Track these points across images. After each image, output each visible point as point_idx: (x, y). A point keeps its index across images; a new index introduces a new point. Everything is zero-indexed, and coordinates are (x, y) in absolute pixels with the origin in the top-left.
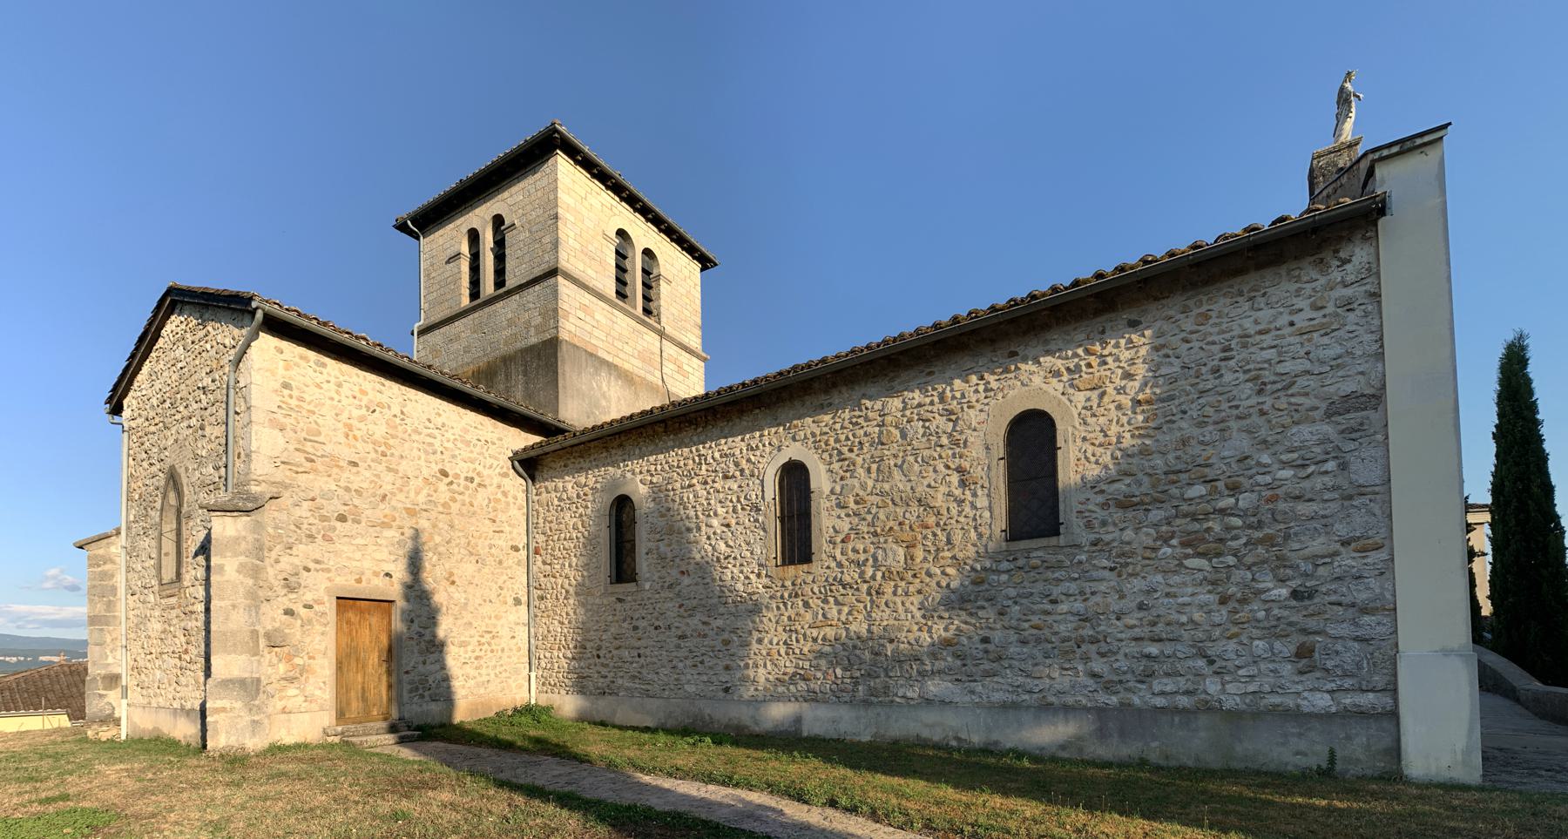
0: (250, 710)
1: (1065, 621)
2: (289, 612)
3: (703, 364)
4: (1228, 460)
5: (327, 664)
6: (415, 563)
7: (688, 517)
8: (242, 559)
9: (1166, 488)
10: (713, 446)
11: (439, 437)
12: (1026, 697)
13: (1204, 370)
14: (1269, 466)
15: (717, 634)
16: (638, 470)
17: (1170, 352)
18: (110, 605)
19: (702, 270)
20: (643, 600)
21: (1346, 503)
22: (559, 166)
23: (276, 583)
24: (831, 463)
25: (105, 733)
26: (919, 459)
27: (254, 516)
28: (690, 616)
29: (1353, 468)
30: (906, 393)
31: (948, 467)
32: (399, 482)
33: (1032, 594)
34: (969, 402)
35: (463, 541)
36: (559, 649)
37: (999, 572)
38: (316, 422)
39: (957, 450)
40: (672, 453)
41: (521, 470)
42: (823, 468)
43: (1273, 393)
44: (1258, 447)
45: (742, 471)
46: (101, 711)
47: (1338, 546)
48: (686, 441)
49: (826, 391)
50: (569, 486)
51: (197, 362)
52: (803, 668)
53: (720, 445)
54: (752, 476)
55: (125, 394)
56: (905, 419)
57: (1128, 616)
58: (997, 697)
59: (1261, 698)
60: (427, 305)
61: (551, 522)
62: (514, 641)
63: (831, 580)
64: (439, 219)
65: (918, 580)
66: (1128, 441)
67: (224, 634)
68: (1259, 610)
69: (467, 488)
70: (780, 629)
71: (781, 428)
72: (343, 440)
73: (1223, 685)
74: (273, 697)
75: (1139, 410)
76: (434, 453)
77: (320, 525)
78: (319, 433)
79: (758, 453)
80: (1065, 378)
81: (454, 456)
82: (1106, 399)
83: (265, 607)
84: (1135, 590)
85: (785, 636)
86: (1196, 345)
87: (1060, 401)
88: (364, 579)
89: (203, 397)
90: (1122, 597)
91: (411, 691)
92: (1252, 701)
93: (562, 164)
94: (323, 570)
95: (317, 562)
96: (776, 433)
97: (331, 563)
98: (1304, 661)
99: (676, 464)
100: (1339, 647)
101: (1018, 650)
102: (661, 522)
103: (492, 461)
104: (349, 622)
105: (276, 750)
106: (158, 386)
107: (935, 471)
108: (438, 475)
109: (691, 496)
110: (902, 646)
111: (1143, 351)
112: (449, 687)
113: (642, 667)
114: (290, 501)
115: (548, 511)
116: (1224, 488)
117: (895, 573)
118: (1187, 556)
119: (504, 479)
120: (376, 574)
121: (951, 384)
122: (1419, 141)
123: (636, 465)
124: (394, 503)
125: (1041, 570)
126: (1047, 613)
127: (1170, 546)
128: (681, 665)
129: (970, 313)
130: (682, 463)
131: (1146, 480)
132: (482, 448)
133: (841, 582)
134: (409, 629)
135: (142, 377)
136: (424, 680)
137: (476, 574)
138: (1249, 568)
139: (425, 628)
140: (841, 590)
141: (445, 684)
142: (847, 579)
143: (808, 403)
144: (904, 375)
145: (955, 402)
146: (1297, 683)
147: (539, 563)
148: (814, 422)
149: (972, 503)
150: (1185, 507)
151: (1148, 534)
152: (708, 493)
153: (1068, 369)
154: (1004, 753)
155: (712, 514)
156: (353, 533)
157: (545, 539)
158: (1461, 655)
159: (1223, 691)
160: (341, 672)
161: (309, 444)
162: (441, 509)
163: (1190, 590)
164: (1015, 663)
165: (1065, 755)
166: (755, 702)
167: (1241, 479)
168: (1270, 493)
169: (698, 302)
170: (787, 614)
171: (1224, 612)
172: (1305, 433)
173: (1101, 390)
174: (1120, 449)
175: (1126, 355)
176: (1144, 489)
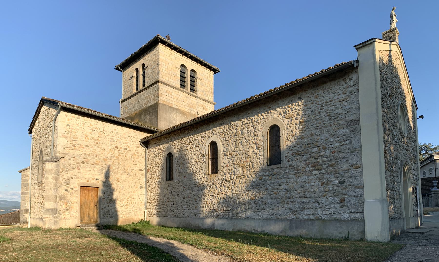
0: (54, 218)
1: (282, 191)
2: (66, 190)
3: (214, 106)
4: (323, 140)
5: (77, 206)
6: (107, 175)
7: (186, 159)
8: (53, 175)
9: (308, 149)
11: (115, 137)
12: (272, 216)
13: (317, 112)
14: (333, 142)
15: (193, 197)
16: (174, 145)
17: (308, 107)
18: (27, 189)
19: (214, 74)
21: (352, 153)
22: (160, 48)
23: (62, 182)
24: (223, 142)
25: (24, 226)
26: (246, 140)
27: (57, 163)
28: (187, 191)
29: (353, 142)
30: (243, 120)
31: (253, 143)
32: (102, 151)
33: (274, 183)
34: (259, 122)
35: (123, 168)
36: (153, 203)
37: (266, 176)
38: (76, 135)
39: (256, 137)
42: (221, 143)
43: (334, 119)
44: (330, 136)
45: (200, 144)
46: (24, 219)
47: (350, 167)
48: (186, 135)
49: (222, 119)
50: (157, 150)
51: (48, 119)
52: (215, 208)
54: (203, 146)
55: (33, 128)
56: (242, 128)
57: (298, 190)
58: (265, 216)
59: (332, 215)
61: (152, 161)
62: (140, 200)
63: (223, 179)
64: (128, 65)
65: (245, 179)
66: (298, 134)
67: (48, 196)
68: (331, 187)
70: (210, 195)
71: (210, 131)
72: (84, 140)
73: (322, 211)
74: (61, 214)
75: (301, 124)
76: (114, 141)
77: (76, 165)
78: (77, 138)
79: (204, 139)
80: (283, 115)
81: (120, 142)
82: (293, 121)
83: (59, 189)
84: (300, 181)
85: (211, 197)
86: (315, 105)
87: (281, 122)
88: (89, 180)
89: (48, 129)
90: (297, 183)
91: (103, 215)
92: (329, 216)
93: (161, 47)
94: (77, 178)
95: (75, 176)
96: (209, 132)
97: (79, 176)
98: (342, 203)
99: (183, 143)
100: (350, 199)
101: (270, 201)
102: (179, 161)
104: (85, 194)
105: (61, 229)
106: (40, 126)
107: (250, 144)
108: (115, 148)
109: (187, 153)
110: (241, 200)
111: (302, 107)
112: (117, 214)
113: (174, 208)
114: (68, 158)
116: (322, 149)
117: (239, 177)
118: (313, 170)
119: (138, 148)
120: (93, 179)
121: (254, 117)
122: (367, 43)
123: (174, 143)
124: (100, 157)
125: (276, 175)
126: (278, 189)
127: (309, 167)
128: (184, 207)
129: (255, 96)
130: (185, 143)
131: (303, 146)
132: (130, 139)
133: (225, 180)
134: (103, 196)
135: (36, 123)
136: (108, 212)
137: (127, 178)
138: (328, 174)
139: (109, 195)
140: (225, 182)
141: (115, 213)
142: (227, 179)
143: (217, 123)
144: (242, 114)
145: (255, 122)
146: (341, 210)
147: (149, 175)
148: (219, 129)
149: (259, 154)
150: (312, 155)
151: (303, 163)
152: (191, 152)
153: (283, 112)
154: (257, 234)
156: (86, 167)
157: (150, 167)
158: (379, 201)
159: (322, 214)
160: (82, 208)
161: (74, 141)
162: (115, 158)
163: (314, 181)
164: (270, 205)
165: (281, 235)
166: (203, 219)
167: (326, 146)
168: (333, 150)
169: (212, 85)
170: (211, 190)
171: (322, 188)
172: (341, 132)
173: (291, 118)
174: (296, 137)
175: (298, 108)
176: (302, 149)
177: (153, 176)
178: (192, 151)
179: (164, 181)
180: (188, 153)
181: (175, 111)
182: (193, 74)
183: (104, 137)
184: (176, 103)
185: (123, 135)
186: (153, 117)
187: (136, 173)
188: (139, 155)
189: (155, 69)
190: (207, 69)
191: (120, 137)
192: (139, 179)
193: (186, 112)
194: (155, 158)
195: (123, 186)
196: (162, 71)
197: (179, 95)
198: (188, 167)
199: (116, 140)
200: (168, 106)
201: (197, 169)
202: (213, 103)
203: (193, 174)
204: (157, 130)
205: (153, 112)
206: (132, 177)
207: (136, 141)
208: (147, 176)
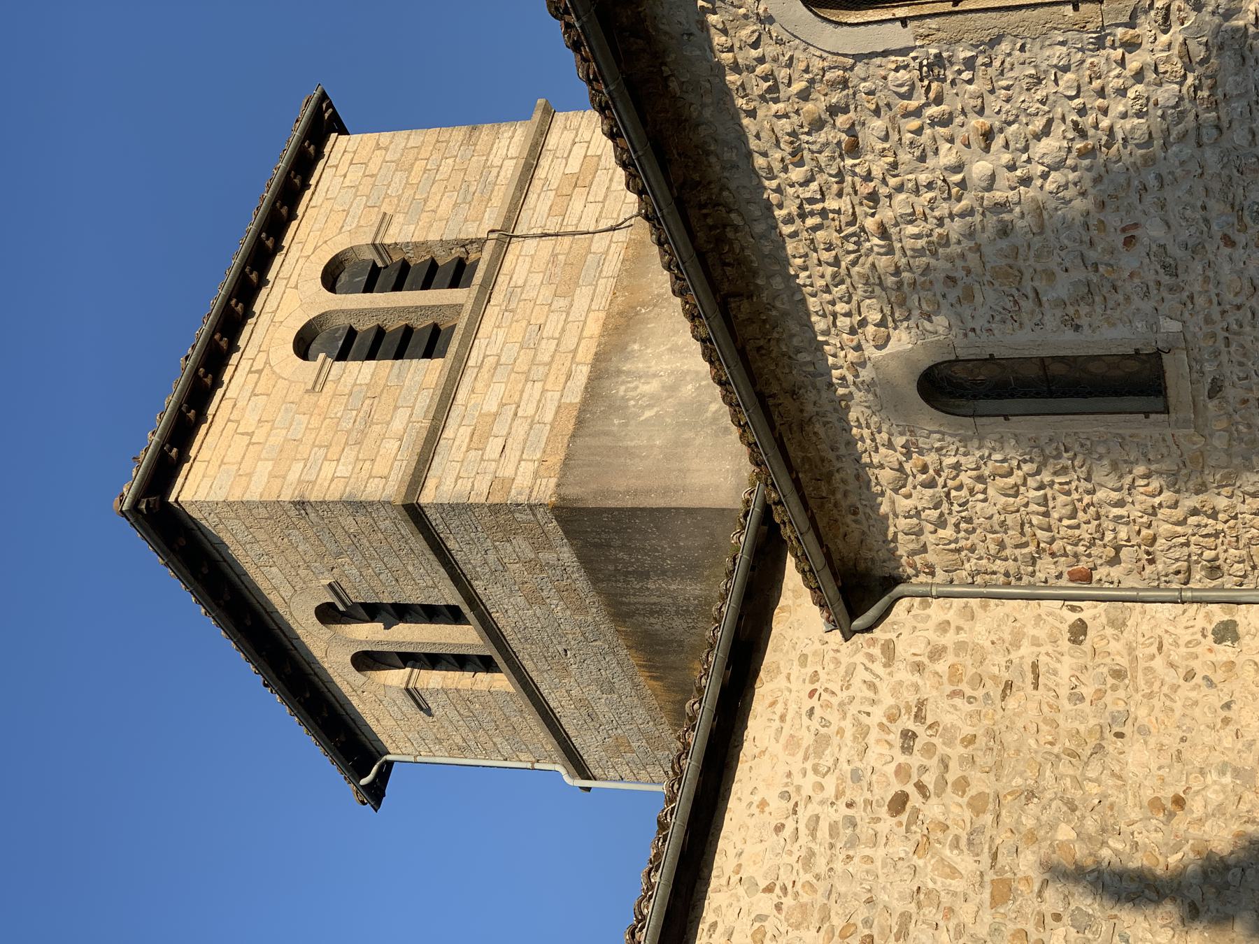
3: (560, 117)
7: (971, 234)
10: (774, 184)
11: (813, 808)
16: (852, 356)
19: (343, 131)
20: (1214, 335)
32: (930, 912)
35: (1064, 768)
40: (803, 278)
41: (872, 613)
45: (833, 110)
48: (767, 248)
50: (904, 504)
53: (770, 169)
54: (845, 83)
60: (523, 756)
61: (1002, 545)
69: (929, 749)
71: (712, 19)
79: (783, 74)
81: (856, 776)
96: (725, 32)
99: (829, 270)
103: (857, 681)
108: (904, 817)
109: (911, 230)
115: (972, 549)
119: (900, 648)
130: (827, 256)
132: (828, 705)
137: (1152, 741)
147: (1116, 572)
155: (957, 178)
157: (1047, 559)
162: (988, 818)
169: (416, 137)
177: (1123, 535)
178: (893, 182)
179: (1168, 432)
180: (911, 219)
181: (606, 383)
182: (353, 275)
183: (822, 887)
184: (551, 378)
185: (801, 754)
186: (665, 544)
187: (1105, 670)
188: (951, 647)
189: (339, 533)
190: (313, 182)
191: (819, 779)
192: (1160, 648)
193: (615, 309)
194: (969, 520)
195: (1222, 773)
196: (342, 482)
197: (498, 363)
198: (1039, 209)
199: (841, 805)
200: (573, 436)
201: (1050, 122)
202: (542, 122)
203: (1101, 158)
204: (755, 510)
205: (623, 547)
206: (1138, 697)
207: (845, 660)
208: (1129, 582)
